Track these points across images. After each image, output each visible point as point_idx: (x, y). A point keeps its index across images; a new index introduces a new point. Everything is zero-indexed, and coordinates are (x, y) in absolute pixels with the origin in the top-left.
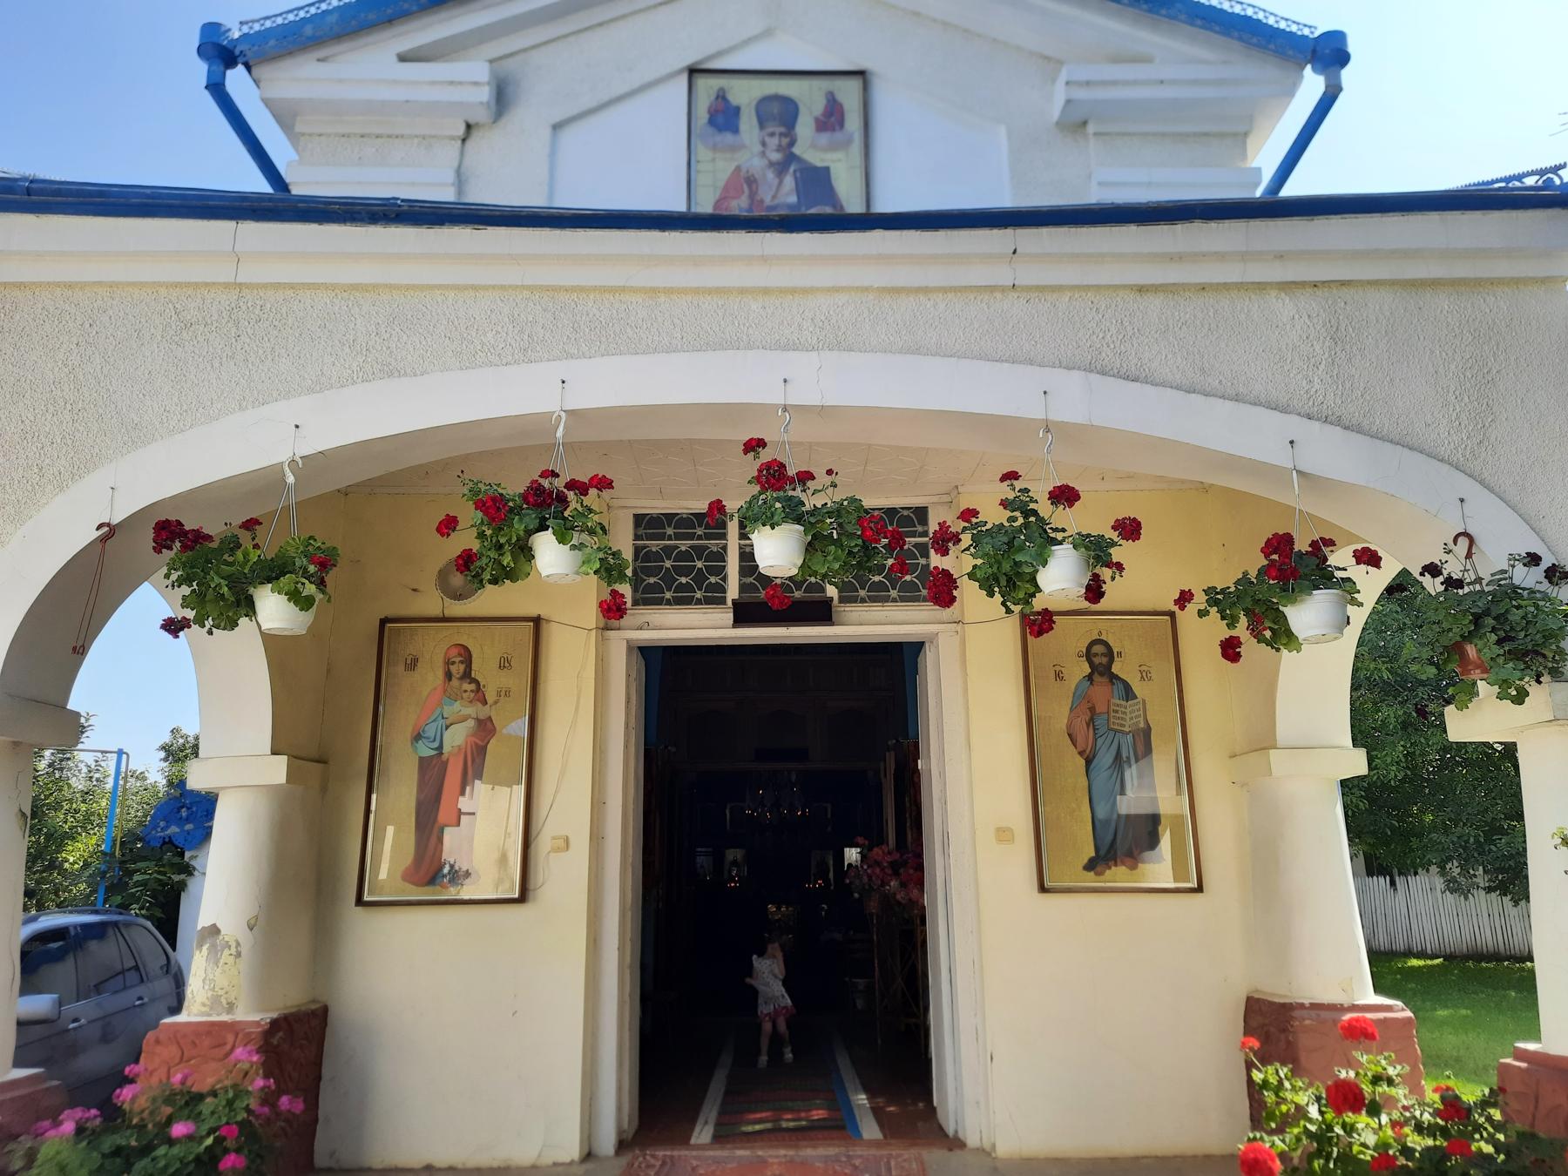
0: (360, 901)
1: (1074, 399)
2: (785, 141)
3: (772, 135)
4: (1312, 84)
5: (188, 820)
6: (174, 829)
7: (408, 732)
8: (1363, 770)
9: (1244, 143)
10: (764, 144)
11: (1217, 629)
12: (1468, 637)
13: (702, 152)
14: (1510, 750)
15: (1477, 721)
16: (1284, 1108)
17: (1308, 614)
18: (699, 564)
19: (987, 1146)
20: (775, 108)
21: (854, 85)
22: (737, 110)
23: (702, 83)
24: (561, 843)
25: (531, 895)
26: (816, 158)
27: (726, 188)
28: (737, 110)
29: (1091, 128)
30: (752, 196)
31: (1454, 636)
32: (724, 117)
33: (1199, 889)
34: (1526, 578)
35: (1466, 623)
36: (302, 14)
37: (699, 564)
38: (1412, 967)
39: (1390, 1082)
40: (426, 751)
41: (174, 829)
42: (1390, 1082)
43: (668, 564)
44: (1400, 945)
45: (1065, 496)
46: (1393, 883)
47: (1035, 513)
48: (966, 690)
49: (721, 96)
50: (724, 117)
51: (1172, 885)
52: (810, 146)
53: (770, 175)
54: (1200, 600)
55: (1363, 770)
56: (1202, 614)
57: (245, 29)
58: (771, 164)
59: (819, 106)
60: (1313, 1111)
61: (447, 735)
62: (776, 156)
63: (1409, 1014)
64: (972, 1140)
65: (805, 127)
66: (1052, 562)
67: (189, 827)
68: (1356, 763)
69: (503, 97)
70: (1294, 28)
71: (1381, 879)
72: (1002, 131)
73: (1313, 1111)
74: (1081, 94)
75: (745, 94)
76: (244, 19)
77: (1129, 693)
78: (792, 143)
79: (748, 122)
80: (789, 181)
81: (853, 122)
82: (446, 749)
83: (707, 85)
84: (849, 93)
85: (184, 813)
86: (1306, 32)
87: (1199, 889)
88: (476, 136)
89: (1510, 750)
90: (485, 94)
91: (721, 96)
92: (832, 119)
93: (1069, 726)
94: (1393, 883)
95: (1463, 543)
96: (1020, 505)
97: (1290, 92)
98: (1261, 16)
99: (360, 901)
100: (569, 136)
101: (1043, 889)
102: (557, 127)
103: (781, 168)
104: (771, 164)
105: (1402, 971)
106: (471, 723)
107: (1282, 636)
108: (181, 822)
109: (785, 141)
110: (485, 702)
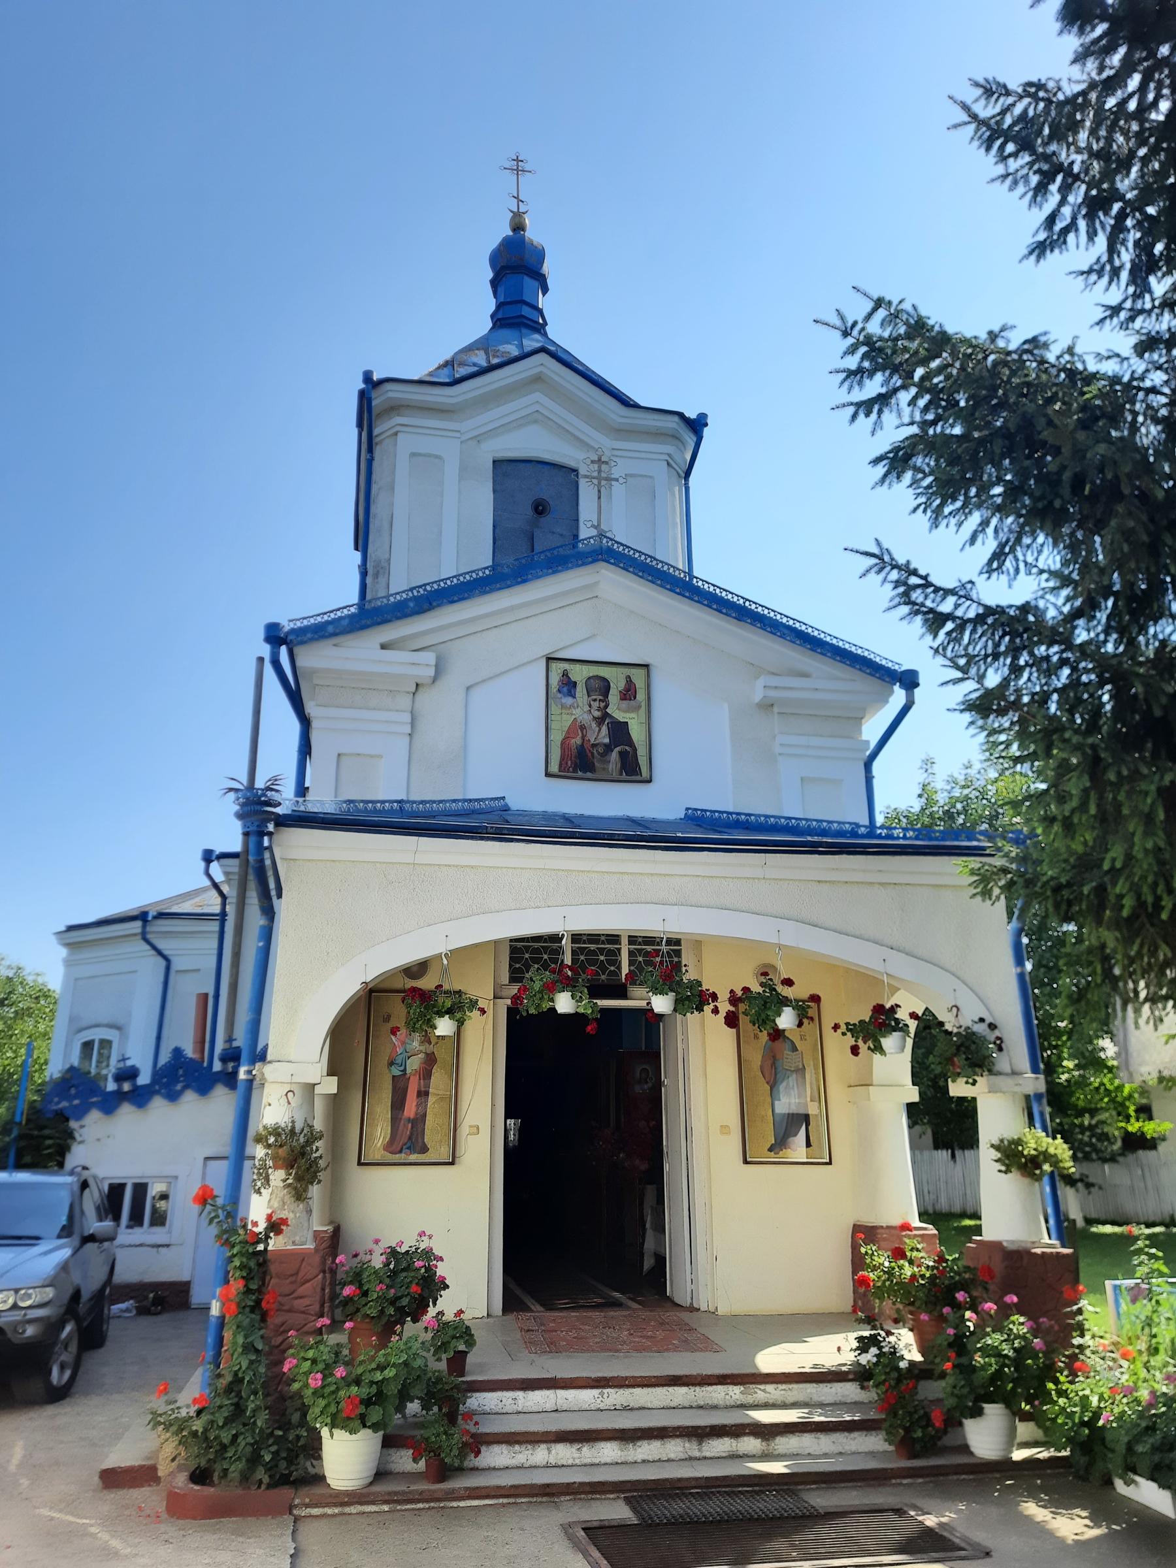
0: (360, 1164)
1: (793, 936)
2: (602, 705)
3: (595, 700)
4: (899, 696)
5: (75, 1097)
6: (64, 1104)
7: (385, 1061)
8: (916, 1099)
9: (861, 725)
10: (590, 706)
11: (850, 1040)
12: (955, 1055)
13: (554, 709)
14: (974, 1099)
15: (958, 1089)
16: (992, 358)
17: (889, 1042)
18: (546, 957)
19: (712, 1309)
20: (596, 684)
21: (642, 672)
22: (575, 683)
23: (554, 665)
24: (475, 1130)
25: (457, 1160)
26: (620, 716)
27: (568, 732)
28: (575, 683)
29: (776, 709)
30: (583, 737)
31: (948, 1054)
32: (568, 685)
33: (830, 1163)
34: (980, 1029)
35: (953, 1049)
36: (326, 618)
37: (546, 957)
38: (965, 1227)
39: (918, 1250)
40: (396, 1071)
41: (64, 1104)
42: (918, 1250)
43: (527, 956)
44: (957, 1209)
45: (788, 982)
46: (953, 1156)
47: (775, 990)
48: (704, 1043)
49: (565, 674)
50: (568, 685)
51: (805, 1160)
52: (617, 711)
53: (594, 725)
54: (843, 1028)
55: (916, 1099)
56: (844, 1034)
57: (292, 625)
58: (595, 718)
59: (622, 685)
60: (887, 1264)
61: (408, 1062)
62: (597, 714)
63: (936, 1232)
64: (703, 1307)
65: (614, 697)
66: (783, 1015)
67: (76, 1102)
68: (913, 1095)
69: (439, 670)
70: (890, 665)
71: (944, 1152)
72: (726, 706)
73: (887, 1264)
74: (772, 693)
75: (579, 674)
76: (291, 618)
77: (794, 1049)
78: (607, 706)
79: (581, 691)
80: (604, 729)
81: (641, 696)
82: (408, 1071)
83: (557, 669)
84: (638, 677)
85: (73, 1091)
86: (897, 667)
87: (830, 1163)
88: (420, 689)
89: (974, 1099)
90: (431, 672)
91: (565, 674)
92: (629, 693)
93: (761, 1067)
94: (953, 1156)
95: (955, 1010)
96: (769, 986)
97: (884, 700)
98: (872, 656)
99: (360, 1164)
100: (476, 694)
101: (746, 1162)
102: (468, 688)
103: (600, 721)
104: (595, 718)
105: (956, 1229)
106: (422, 1056)
107: (878, 1048)
108: (70, 1098)
109: (602, 705)
110: (430, 1043)
